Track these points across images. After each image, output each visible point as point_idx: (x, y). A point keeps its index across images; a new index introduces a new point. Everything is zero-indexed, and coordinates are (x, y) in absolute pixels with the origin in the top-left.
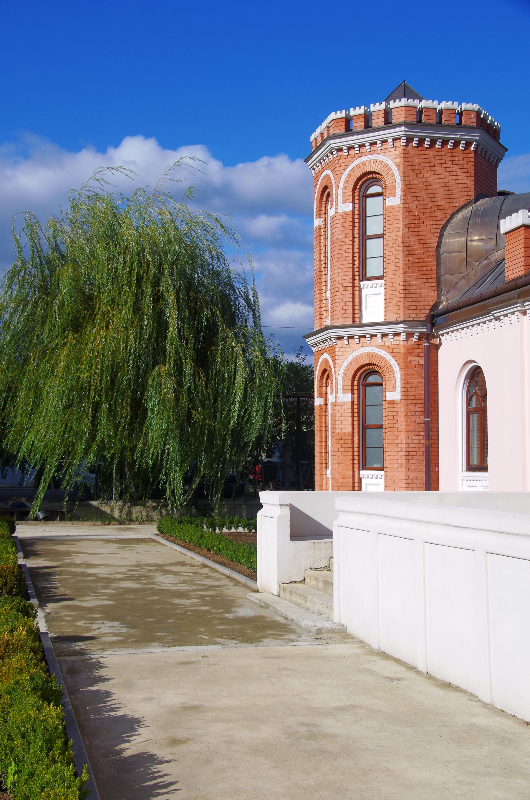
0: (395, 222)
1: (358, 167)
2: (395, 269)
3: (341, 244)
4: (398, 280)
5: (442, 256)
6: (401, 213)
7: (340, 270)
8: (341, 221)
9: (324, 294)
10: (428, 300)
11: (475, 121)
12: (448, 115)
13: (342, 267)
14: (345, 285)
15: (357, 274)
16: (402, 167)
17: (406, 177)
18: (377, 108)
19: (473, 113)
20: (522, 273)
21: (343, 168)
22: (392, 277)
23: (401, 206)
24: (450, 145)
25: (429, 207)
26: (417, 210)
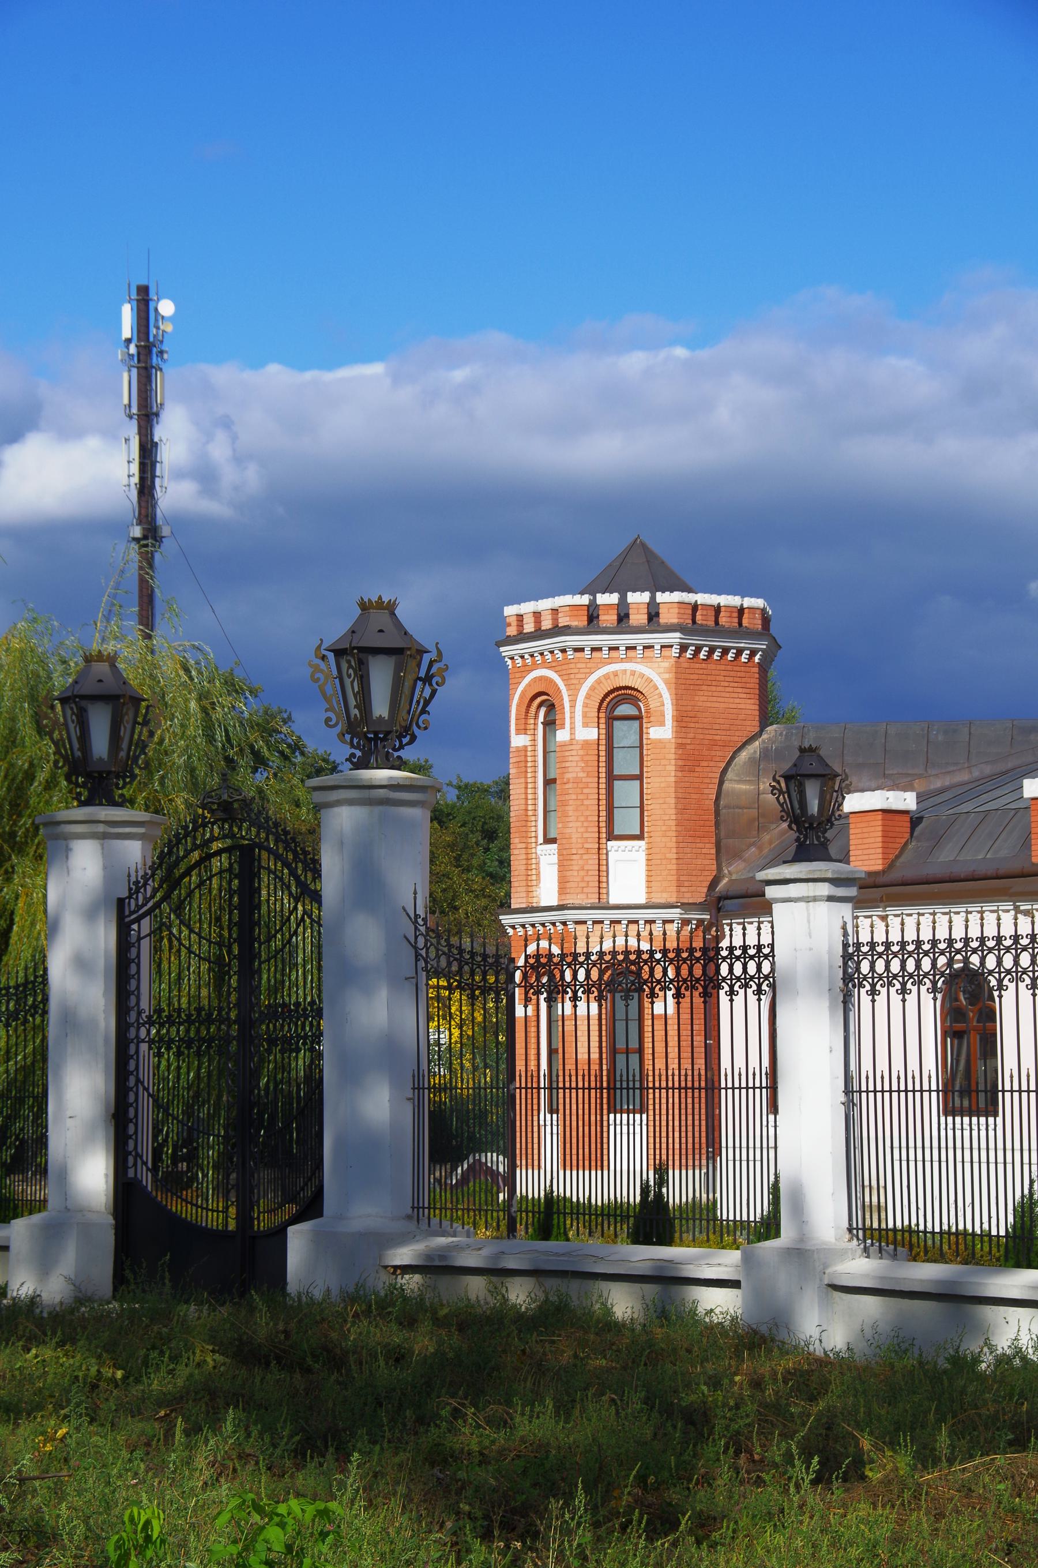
0: (663, 762)
1: (607, 676)
2: (664, 828)
3: (580, 785)
4: (670, 845)
5: (723, 812)
6: (673, 751)
7: (579, 824)
8: (581, 752)
9: (533, 850)
10: (706, 873)
11: (760, 622)
12: (728, 614)
13: (582, 819)
14: (586, 846)
15: (604, 830)
16: (673, 686)
17: (679, 700)
18: (638, 598)
19: (758, 612)
20: (880, 868)
21: (583, 676)
22: (658, 840)
23: (673, 741)
24: (731, 656)
25: (706, 742)
26: (692, 747)
